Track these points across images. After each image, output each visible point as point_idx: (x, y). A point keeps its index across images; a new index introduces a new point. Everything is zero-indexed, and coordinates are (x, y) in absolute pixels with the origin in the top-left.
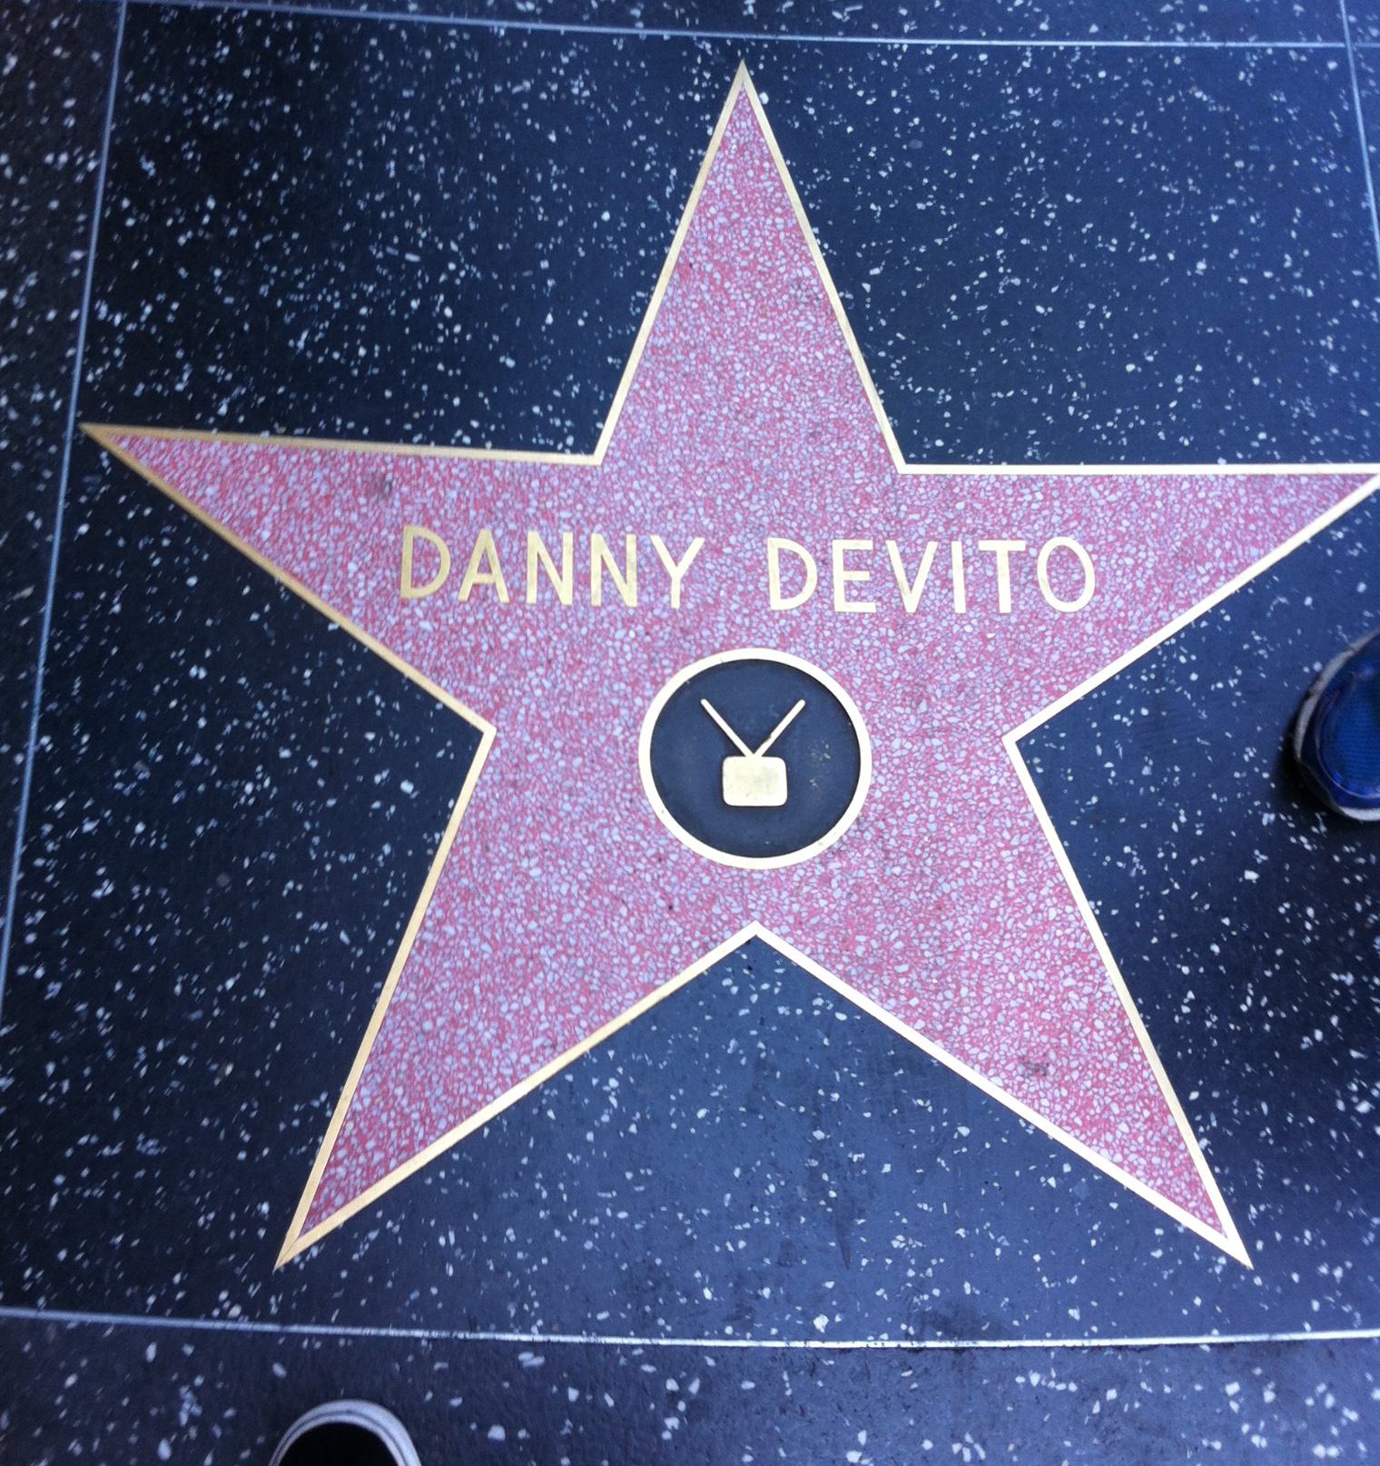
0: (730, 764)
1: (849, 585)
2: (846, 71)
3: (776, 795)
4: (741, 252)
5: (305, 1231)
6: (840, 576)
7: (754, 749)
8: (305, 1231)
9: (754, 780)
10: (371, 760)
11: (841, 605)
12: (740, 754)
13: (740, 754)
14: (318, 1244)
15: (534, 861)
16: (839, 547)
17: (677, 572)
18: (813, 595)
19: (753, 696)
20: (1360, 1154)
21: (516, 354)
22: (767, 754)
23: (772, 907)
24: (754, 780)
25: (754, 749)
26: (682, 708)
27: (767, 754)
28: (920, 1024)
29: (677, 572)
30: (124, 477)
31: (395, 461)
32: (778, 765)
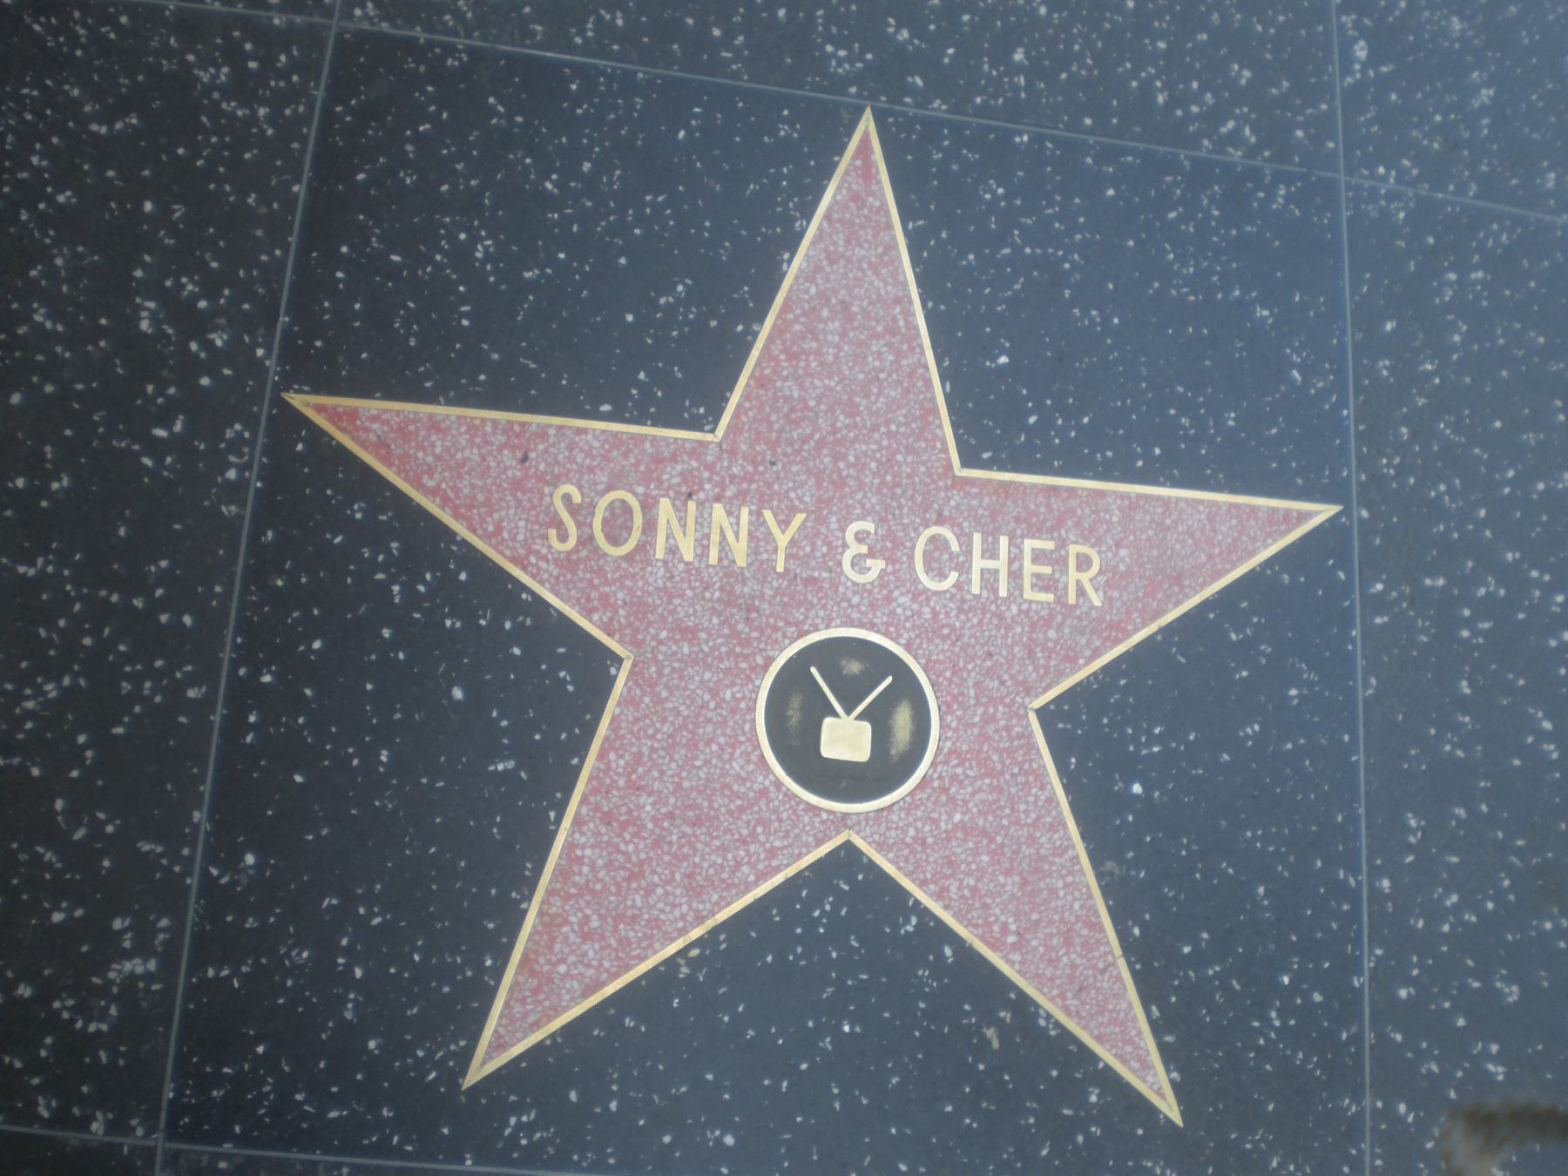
0: (828, 721)
2: (1315, 1069)
4: (852, 257)
7: (848, 712)
9: (845, 738)
12: (835, 714)
13: (835, 714)
14: (1168, 1071)
15: (651, 800)
17: (783, 540)
19: (856, 672)
20: (575, 228)
21: (652, 335)
22: (857, 718)
24: (845, 738)
25: (848, 712)
26: (793, 678)
27: (857, 718)
29: (783, 540)
30: (300, 420)
31: (1060, 851)
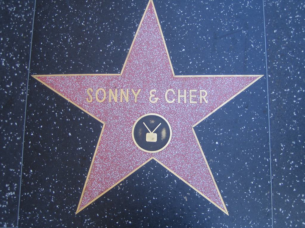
0: (147, 134)
1: (193, 98)
3: (155, 140)
5: (258, 77)
6: (191, 96)
8: (258, 77)
9: (151, 137)
10: (89, 129)
11: (191, 102)
12: (149, 132)
13: (149, 132)
16: (191, 91)
17: (136, 96)
18: (154, 103)
23: (155, 155)
24: (151, 137)
26: (140, 124)
28: (224, 102)
29: (136, 96)
32: (156, 134)
